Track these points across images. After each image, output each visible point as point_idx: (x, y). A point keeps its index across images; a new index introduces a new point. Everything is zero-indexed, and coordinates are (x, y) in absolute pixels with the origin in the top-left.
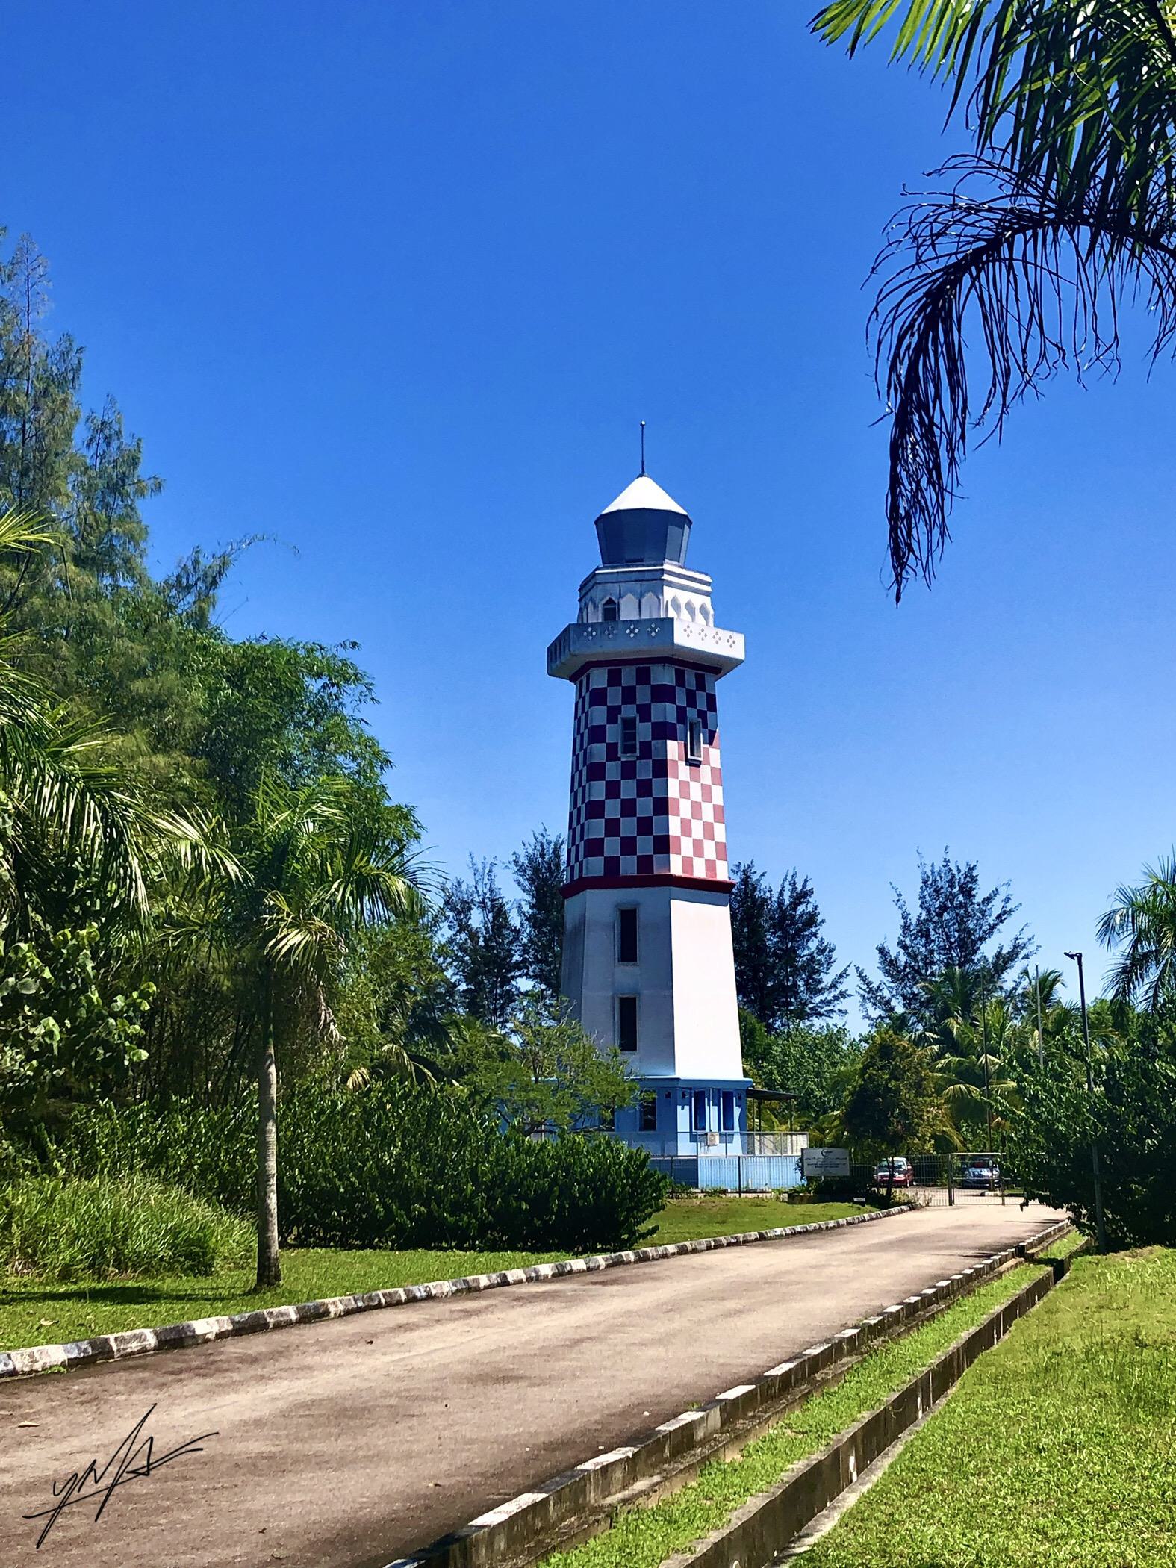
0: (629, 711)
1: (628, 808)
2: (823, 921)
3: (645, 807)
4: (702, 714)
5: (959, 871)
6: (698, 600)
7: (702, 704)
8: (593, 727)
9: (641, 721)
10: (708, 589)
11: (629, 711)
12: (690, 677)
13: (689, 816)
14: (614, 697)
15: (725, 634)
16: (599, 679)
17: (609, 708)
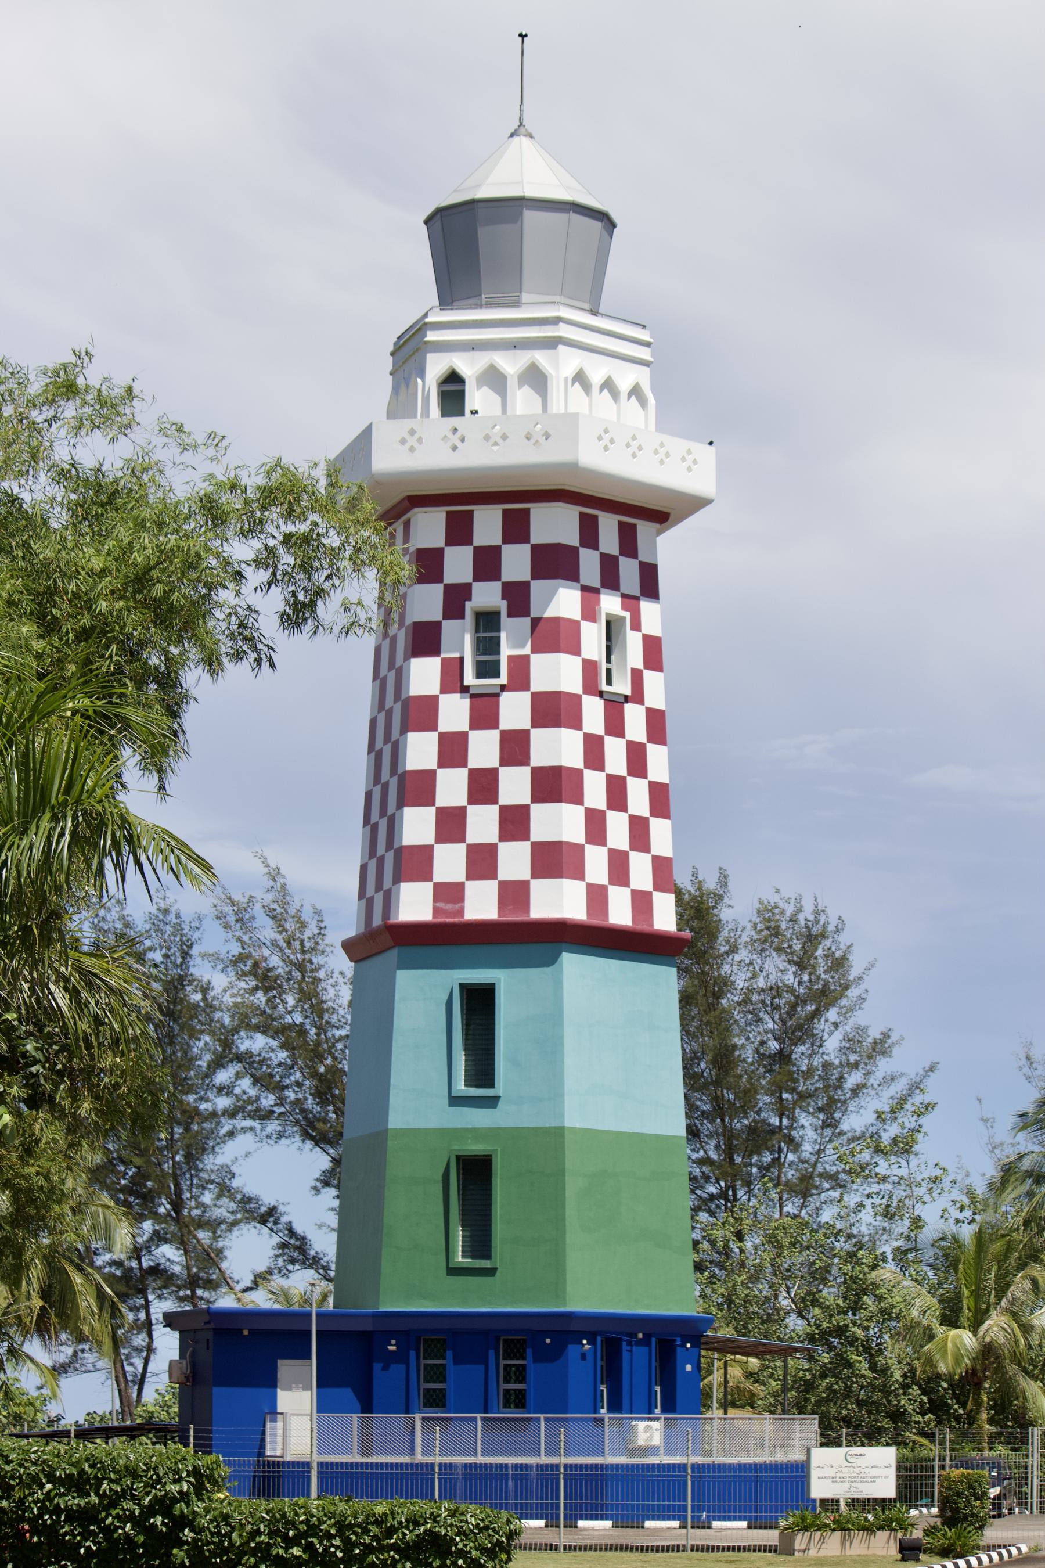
0: (487, 596)
2: (724, 880)
6: (627, 377)
8: (417, 625)
9: (510, 615)
10: (645, 354)
11: (487, 596)
12: (608, 526)
14: (458, 565)
15: (677, 446)
16: (429, 528)
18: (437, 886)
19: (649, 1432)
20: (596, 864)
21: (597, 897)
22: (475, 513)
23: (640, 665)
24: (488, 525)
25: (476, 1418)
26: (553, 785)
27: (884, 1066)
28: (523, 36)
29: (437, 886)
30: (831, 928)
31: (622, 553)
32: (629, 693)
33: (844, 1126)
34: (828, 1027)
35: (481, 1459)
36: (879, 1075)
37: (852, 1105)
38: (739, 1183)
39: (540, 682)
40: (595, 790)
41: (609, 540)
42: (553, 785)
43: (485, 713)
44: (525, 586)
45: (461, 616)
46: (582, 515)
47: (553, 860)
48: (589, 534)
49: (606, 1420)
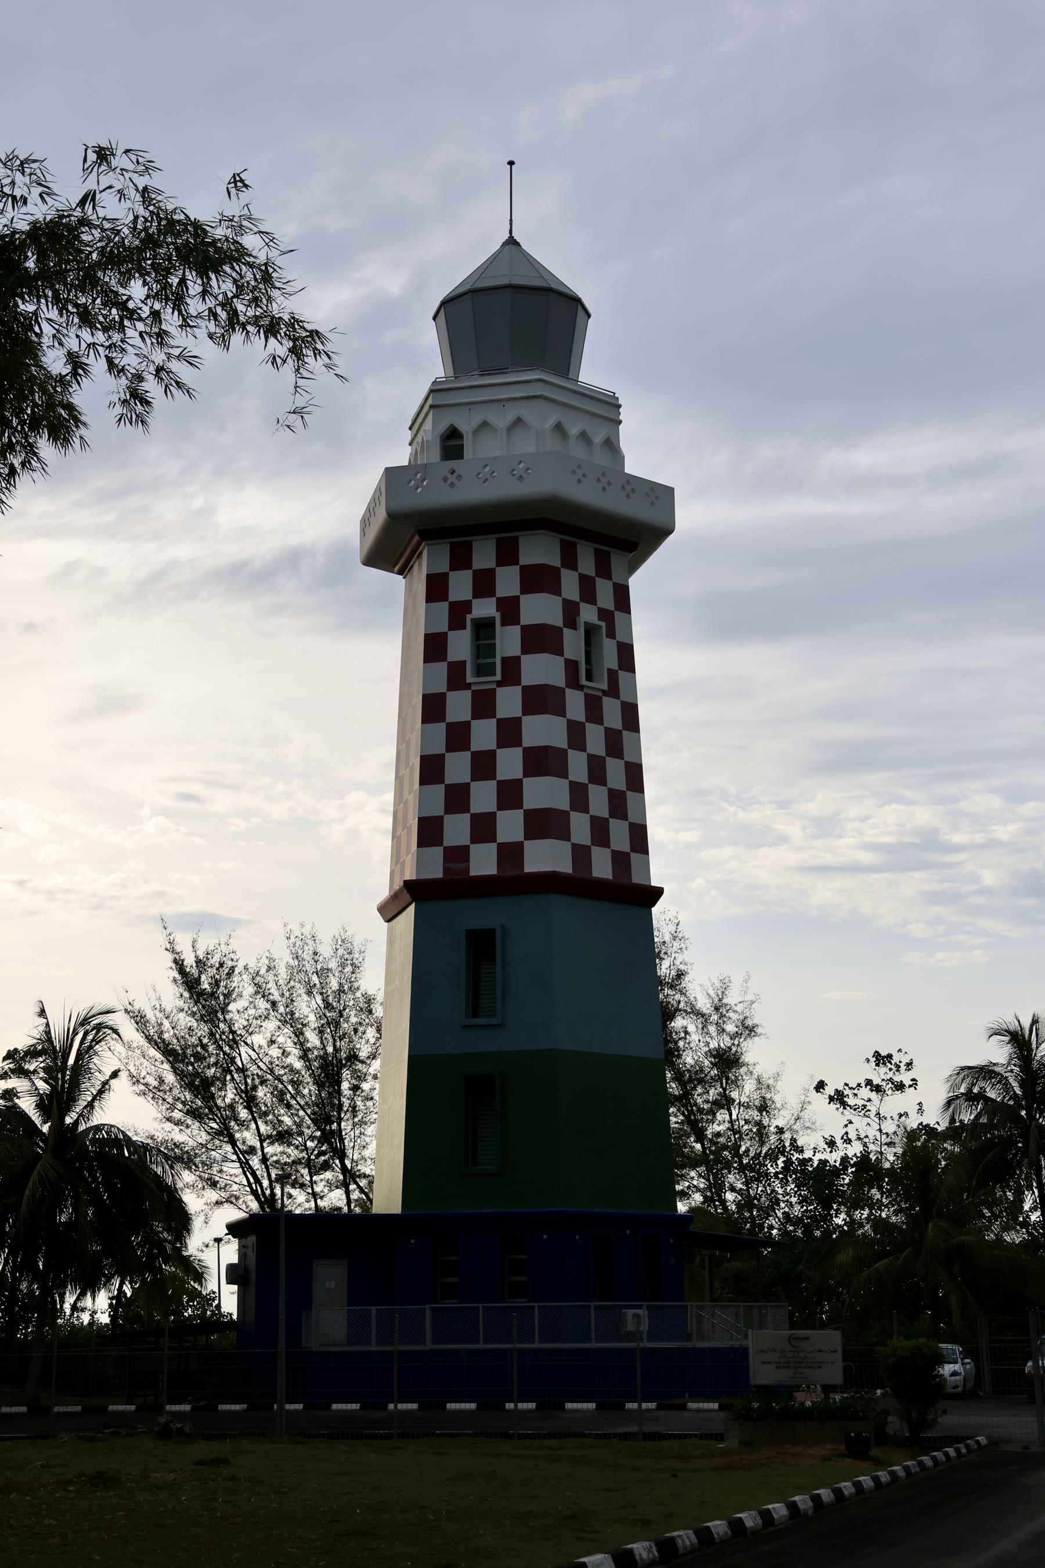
0: (485, 608)
1: (484, 766)
3: (458, 768)
4: (605, 615)
5: (7, 488)
7: (612, 716)
11: (485, 608)
13: (586, 841)
17: (452, 605)
18: (447, 850)
19: (636, 1317)
20: (580, 828)
21: (581, 855)
22: (474, 544)
25: (589, 1307)
26: (543, 762)
29: (447, 850)
31: (582, 725)
32: (606, 688)
35: (481, 1346)
39: (531, 801)
40: (578, 766)
42: (543, 762)
43: (484, 705)
44: (515, 600)
47: (544, 824)
49: (593, 1308)
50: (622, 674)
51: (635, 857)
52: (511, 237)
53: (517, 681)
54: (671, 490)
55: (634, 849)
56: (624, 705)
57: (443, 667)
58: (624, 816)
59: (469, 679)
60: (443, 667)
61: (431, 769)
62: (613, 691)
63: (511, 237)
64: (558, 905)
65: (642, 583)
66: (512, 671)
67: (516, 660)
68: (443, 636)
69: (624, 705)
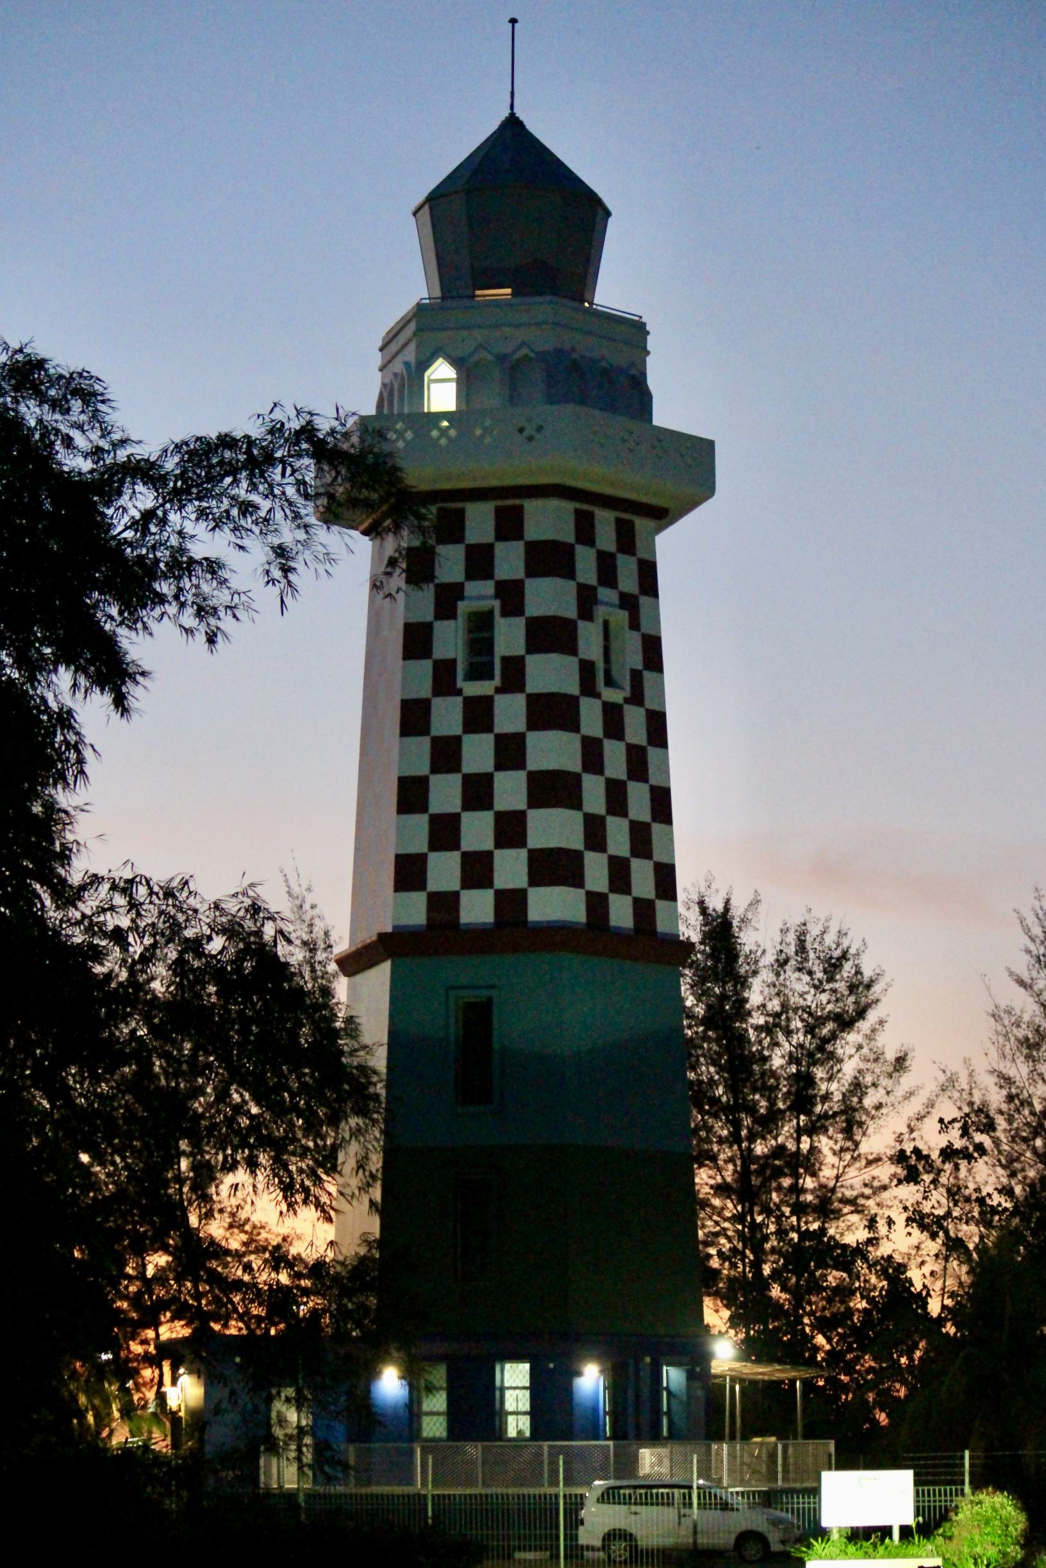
1: (478, 792)
7: (635, 727)
9: (504, 614)
11: (480, 594)
12: (605, 522)
21: (597, 904)
23: (640, 667)
24: (480, 522)
26: (552, 789)
27: (907, 1081)
28: (513, 21)
30: (852, 951)
33: (864, 1148)
34: (850, 1050)
36: (899, 1092)
37: (872, 1127)
38: (756, 1209)
41: (606, 538)
42: (552, 789)
43: (478, 715)
45: (454, 616)
46: (577, 512)
47: (555, 867)
48: (585, 530)
50: (648, 675)
51: (657, 828)
52: (512, 115)
53: (520, 688)
54: (710, 444)
55: (660, 895)
56: (653, 789)
57: (427, 666)
58: (647, 854)
59: (460, 683)
60: (427, 666)
61: (412, 795)
62: (637, 697)
63: (512, 115)
64: (572, 962)
65: (673, 548)
66: (514, 676)
67: (520, 660)
68: (428, 627)
69: (653, 789)
